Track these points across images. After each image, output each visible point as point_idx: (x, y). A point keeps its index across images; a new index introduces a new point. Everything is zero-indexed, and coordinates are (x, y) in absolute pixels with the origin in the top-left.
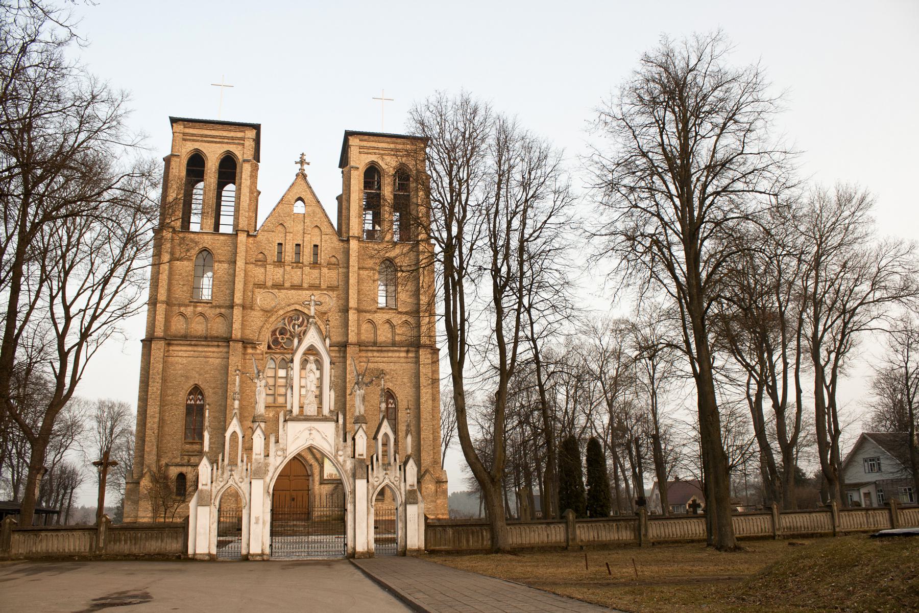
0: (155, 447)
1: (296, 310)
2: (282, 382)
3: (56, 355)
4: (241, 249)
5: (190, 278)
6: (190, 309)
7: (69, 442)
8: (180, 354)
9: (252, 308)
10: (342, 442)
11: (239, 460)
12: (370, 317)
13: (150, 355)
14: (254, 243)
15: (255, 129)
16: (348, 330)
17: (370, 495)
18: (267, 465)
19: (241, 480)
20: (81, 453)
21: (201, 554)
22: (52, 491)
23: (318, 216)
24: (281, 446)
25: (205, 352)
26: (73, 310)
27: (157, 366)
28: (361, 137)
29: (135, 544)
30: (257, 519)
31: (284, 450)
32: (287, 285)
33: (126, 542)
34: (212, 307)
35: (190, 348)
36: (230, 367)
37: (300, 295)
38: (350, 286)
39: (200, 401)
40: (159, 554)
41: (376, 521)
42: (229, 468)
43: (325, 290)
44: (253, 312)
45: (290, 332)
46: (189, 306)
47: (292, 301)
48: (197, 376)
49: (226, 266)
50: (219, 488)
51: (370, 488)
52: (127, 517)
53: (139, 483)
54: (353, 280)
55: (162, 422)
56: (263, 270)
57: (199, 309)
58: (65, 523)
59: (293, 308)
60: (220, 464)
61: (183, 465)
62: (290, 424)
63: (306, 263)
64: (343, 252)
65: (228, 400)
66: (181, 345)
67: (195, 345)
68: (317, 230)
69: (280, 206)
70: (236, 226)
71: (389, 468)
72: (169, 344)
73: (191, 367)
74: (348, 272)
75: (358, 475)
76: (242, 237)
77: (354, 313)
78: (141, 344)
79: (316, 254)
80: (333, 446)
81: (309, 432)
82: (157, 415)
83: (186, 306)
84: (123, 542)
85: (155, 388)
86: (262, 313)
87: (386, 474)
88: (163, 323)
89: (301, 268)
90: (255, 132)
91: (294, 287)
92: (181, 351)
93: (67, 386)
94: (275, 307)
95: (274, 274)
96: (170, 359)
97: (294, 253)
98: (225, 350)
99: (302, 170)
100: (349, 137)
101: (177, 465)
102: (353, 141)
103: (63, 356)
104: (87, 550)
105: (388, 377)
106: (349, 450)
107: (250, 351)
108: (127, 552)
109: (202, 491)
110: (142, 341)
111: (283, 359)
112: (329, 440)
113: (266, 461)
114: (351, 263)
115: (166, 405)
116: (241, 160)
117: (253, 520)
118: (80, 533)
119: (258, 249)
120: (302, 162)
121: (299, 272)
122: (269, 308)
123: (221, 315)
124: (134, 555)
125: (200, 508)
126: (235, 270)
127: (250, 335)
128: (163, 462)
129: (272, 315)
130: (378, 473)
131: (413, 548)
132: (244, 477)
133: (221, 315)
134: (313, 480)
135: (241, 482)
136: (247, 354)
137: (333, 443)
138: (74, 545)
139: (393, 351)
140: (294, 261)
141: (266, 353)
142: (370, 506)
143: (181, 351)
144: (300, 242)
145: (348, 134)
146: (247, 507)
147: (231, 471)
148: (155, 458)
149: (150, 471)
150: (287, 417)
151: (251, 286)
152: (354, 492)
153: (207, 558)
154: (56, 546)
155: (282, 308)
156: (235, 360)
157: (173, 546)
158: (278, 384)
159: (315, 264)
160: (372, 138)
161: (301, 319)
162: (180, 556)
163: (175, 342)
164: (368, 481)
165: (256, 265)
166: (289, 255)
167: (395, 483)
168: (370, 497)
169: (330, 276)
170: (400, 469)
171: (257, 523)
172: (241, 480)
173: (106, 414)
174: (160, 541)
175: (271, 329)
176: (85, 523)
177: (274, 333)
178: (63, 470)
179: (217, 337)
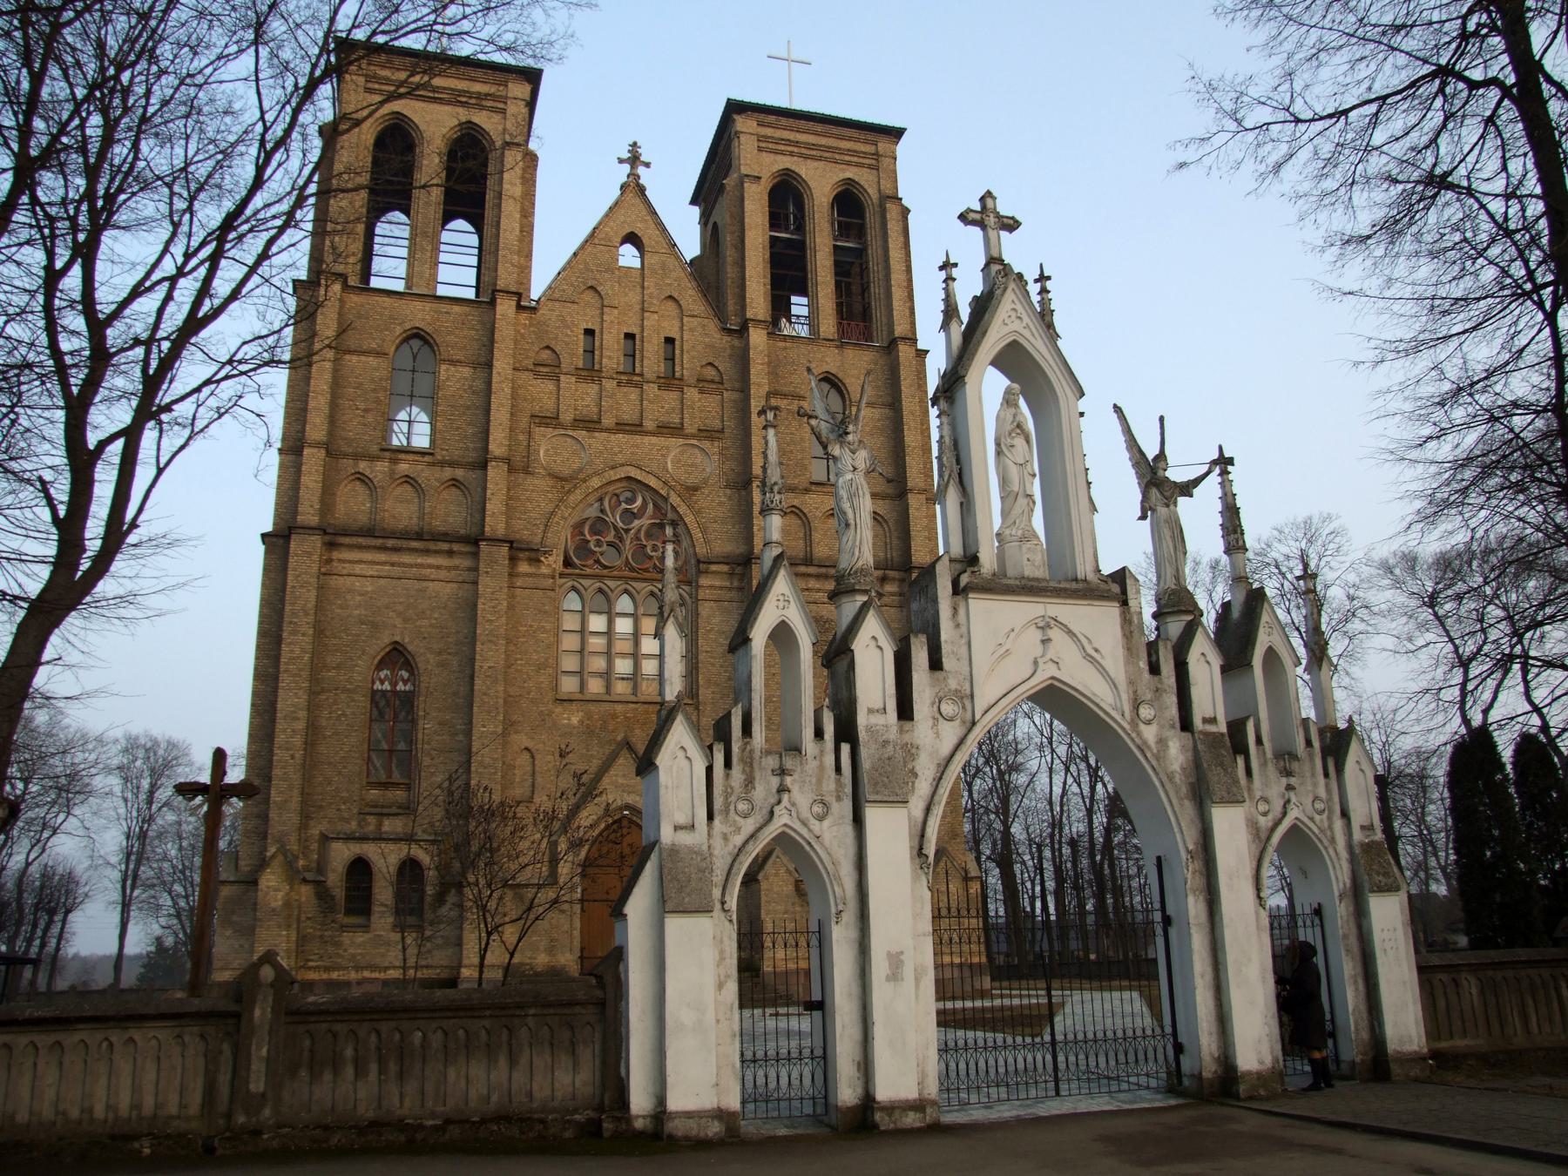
0: (296, 792)
1: (629, 478)
2: (597, 643)
3: (59, 458)
5: (381, 395)
7: (59, 820)
8: (358, 569)
9: (527, 471)
10: (1146, 675)
11: (808, 732)
12: (796, 502)
14: (531, 325)
15: (529, 81)
18: (910, 751)
20: (85, 842)
21: (689, 1115)
22: (19, 923)
23: (674, 274)
24: (953, 684)
25: (421, 566)
26: (115, 335)
27: (302, 596)
28: (762, 116)
29: (401, 1076)
30: (896, 961)
32: (608, 421)
34: (433, 464)
35: (382, 557)
36: (481, 601)
37: (637, 446)
39: (405, 682)
40: (503, 1117)
43: (693, 436)
44: (529, 480)
45: (616, 528)
46: (378, 458)
47: (620, 458)
48: (398, 622)
49: (466, 371)
50: (738, 840)
52: (223, 969)
53: (255, 883)
55: (313, 733)
56: (551, 386)
57: (403, 467)
58: (49, 984)
59: (622, 473)
60: (736, 748)
61: (364, 839)
62: (980, 607)
63: (649, 375)
64: (731, 356)
65: (478, 682)
66: (360, 547)
67: (396, 550)
68: (671, 305)
69: (589, 249)
71: (1295, 766)
72: (331, 546)
79: (670, 359)
82: (303, 714)
83: (373, 458)
84: (349, 1071)
85: (296, 646)
86: (551, 482)
87: (1289, 788)
88: (318, 493)
89: (639, 386)
90: (528, 88)
91: (621, 427)
92: (360, 562)
93: (93, 545)
94: (581, 470)
95: (578, 397)
96: (335, 582)
97: (621, 353)
98: (467, 562)
99: (633, 176)
100: (736, 117)
101: (349, 838)
102: (742, 123)
103: (82, 460)
104: (194, 1107)
107: (524, 567)
108: (366, 1111)
109: (674, 851)
111: (600, 590)
112: (1108, 664)
113: (907, 738)
114: (753, 379)
115: (323, 691)
116: (498, 144)
118: (162, 1033)
120: (634, 159)
121: (634, 394)
122: (566, 472)
123: (455, 483)
124: (400, 1125)
125: (673, 924)
127: (527, 533)
128: (315, 831)
129: (575, 487)
130: (1266, 784)
132: (831, 799)
133: (455, 483)
135: (821, 818)
136: (517, 575)
138: (136, 1089)
140: (621, 369)
141: (562, 575)
143: (360, 562)
144: (635, 330)
145: (734, 109)
146: (850, 916)
147: (782, 772)
148: (296, 819)
149: (283, 850)
150: (964, 579)
151: (524, 422)
153: (714, 1129)
154: (50, 1094)
155: (596, 474)
156: (492, 584)
158: (590, 648)
159: (670, 380)
160: (784, 121)
161: (639, 502)
163: (347, 540)
165: (537, 374)
166: (611, 355)
169: (703, 408)
170: (1326, 775)
171: (895, 976)
172: (818, 809)
173: (138, 763)
174: (503, 1062)
175: (572, 521)
176: (85, 983)
177: (578, 527)
178: (46, 875)
179: (446, 534)
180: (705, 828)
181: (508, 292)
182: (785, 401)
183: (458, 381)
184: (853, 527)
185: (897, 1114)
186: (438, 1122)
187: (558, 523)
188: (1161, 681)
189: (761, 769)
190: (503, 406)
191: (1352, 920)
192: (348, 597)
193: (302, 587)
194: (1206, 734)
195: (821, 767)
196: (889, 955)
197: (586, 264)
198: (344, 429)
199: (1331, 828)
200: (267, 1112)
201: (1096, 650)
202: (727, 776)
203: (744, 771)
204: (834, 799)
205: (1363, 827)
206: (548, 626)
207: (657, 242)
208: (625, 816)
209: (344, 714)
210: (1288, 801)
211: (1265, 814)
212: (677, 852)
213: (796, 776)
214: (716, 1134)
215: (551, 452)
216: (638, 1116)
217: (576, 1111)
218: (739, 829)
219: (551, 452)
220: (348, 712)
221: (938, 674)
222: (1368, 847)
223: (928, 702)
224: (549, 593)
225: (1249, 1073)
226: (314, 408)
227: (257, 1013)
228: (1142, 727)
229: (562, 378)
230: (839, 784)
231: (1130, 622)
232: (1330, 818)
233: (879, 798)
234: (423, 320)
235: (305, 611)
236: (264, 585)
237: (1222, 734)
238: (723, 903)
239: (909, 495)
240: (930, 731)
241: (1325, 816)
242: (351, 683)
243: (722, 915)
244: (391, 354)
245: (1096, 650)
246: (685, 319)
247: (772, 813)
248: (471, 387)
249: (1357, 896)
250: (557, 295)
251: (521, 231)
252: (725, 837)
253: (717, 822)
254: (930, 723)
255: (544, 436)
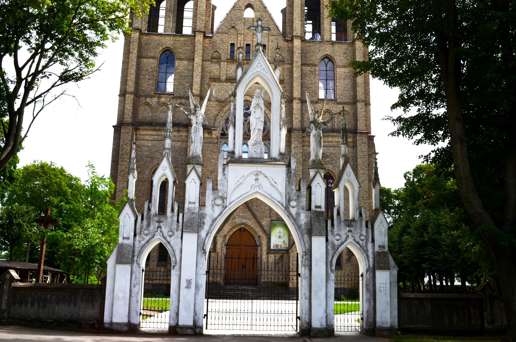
4: (199, 47)
6: (155, 100)
13: (120, 139)
14: (210, 43)
16: (292, 118)
17: (330, 257)
18: (202, 216)
19: (170, 233)
21: (118, 324)
23: (266, 19)
24: (220, 194)
30: (189, 282)
31: (223, 199)
33: (33, 305)
34: (173, 98)
35: (154, 133)
38: (295, 79)
41: (336, 289)
42: (156, 219)
46: (154, 97)
49: (186, 63)
50: (143, 242)
51: (329, 248)
54: (297, 74)
57: (163, 99)
62: (232, 168)
70: (194, 31)
71: (353, 223)
72: (136, 129)
73: (156, 149)
74: (292, 68)
75: (315, 231)
76: (199, 37)
77: (298, 103)
78: (113, 129)
80: (284, 195)
81: (254, 177)
83: (151, 97)
84: (29, 305)
86: (217, 103)
87: (350, 231)
92: (147, 135)
105: (328, 159)
106: (304, 201)
109: (122, 245)
110: (113, 126)
113: (202, 212)
114: (295, 59)
117: (184, 284)
119: (213, 48)
125: (119, 267)
126: (193, 66)
129: (226, 105)
130: (339, 230)
131: (385, 325)
134: (261, 250)
135: (170, 236)
137: (283, 191)
139: (332, 136)
141: (221, 138)
142: (329, 271)
143: (147, 135)
147: (159, 222)
152: (309, 253)
153: (125, 328)
157: (91, 312)
162: (94, 324)
164: (327, 240)
165: (212, 62)
167: (361, 242)
168: (329, 260)
170: (367, 226)
172: (170, 233)
174: (72, 305)
180: (133, 238)
181: (200, 32)
182: (309, 67)
183: (183, 66)
184: (193, 143)
185: (184, 330)
186: (52, 321)
187: (219, 119)
188: (300, 193)
189: (153, 220)
190: (198, 75)
191: (371, 279)
192: (143, 148)
193: (125, 145)
194: (316, 212)
195: (172, 220)
196: (187, 280)
197: (231, 17)
198: (141, 87)
199: (366, 246)
200: (5, 314)
201: (275, 183)
202: (142, 223)
203: (147, 221)
204: (175, 231)
205: (379, 246)
206: (215, 157)
207: (259, 7)
208: (242, 227)
209: (141, 190)
210: (348, 236)
211: (338, 240)
212: (123, 245)
213: (164, 223)
214: (126, 330)
215: (217, 92)
216: (106, 323)
217: (91, 321)
218: (144, 239)
219: (217, 92)
220: (142, 189)
221: (216, 191)
222: (379, 254)
223: (211, 200)
224: (216, 145)
225: (316, 328)
226: (130, 80)
227: (5, 287)
228: (291, 209)
229: (222, 63)
230: (178, 226)
231: (291, 172)
232: (366, 243)
233: (187, 231)
234: (170, 44)
235: (126, 153)
236: (113, 144)
237: (323, 212)
238: (137, 261)
239: (358, 103)
240: (211, 210)
241: (364, 242)
242: (144, 179)
243: (137, 265)
244: (159, 57)
245: (275, 183)
246: (270, 37)
247: (154, 234)
248: (187, 68)
249: (372, 271)
250: (220, 31)
251: (206, 7)
252: (140, 242)
253: (137, 237)
254: (211, 206)
255: (215, 86)
